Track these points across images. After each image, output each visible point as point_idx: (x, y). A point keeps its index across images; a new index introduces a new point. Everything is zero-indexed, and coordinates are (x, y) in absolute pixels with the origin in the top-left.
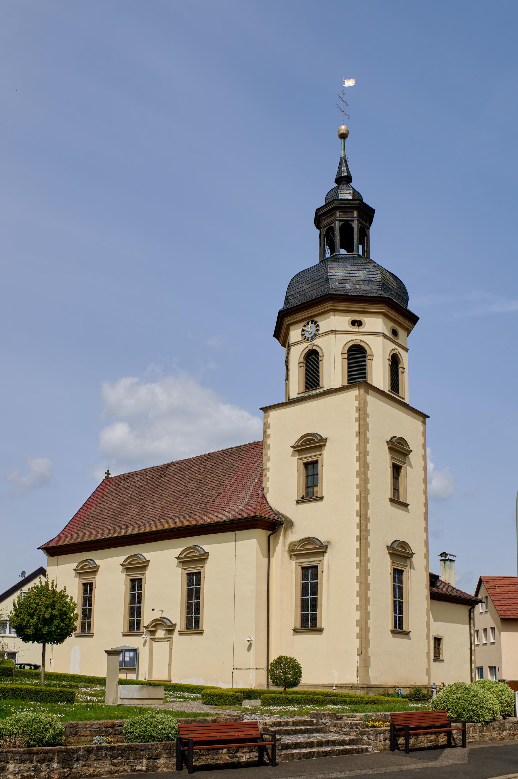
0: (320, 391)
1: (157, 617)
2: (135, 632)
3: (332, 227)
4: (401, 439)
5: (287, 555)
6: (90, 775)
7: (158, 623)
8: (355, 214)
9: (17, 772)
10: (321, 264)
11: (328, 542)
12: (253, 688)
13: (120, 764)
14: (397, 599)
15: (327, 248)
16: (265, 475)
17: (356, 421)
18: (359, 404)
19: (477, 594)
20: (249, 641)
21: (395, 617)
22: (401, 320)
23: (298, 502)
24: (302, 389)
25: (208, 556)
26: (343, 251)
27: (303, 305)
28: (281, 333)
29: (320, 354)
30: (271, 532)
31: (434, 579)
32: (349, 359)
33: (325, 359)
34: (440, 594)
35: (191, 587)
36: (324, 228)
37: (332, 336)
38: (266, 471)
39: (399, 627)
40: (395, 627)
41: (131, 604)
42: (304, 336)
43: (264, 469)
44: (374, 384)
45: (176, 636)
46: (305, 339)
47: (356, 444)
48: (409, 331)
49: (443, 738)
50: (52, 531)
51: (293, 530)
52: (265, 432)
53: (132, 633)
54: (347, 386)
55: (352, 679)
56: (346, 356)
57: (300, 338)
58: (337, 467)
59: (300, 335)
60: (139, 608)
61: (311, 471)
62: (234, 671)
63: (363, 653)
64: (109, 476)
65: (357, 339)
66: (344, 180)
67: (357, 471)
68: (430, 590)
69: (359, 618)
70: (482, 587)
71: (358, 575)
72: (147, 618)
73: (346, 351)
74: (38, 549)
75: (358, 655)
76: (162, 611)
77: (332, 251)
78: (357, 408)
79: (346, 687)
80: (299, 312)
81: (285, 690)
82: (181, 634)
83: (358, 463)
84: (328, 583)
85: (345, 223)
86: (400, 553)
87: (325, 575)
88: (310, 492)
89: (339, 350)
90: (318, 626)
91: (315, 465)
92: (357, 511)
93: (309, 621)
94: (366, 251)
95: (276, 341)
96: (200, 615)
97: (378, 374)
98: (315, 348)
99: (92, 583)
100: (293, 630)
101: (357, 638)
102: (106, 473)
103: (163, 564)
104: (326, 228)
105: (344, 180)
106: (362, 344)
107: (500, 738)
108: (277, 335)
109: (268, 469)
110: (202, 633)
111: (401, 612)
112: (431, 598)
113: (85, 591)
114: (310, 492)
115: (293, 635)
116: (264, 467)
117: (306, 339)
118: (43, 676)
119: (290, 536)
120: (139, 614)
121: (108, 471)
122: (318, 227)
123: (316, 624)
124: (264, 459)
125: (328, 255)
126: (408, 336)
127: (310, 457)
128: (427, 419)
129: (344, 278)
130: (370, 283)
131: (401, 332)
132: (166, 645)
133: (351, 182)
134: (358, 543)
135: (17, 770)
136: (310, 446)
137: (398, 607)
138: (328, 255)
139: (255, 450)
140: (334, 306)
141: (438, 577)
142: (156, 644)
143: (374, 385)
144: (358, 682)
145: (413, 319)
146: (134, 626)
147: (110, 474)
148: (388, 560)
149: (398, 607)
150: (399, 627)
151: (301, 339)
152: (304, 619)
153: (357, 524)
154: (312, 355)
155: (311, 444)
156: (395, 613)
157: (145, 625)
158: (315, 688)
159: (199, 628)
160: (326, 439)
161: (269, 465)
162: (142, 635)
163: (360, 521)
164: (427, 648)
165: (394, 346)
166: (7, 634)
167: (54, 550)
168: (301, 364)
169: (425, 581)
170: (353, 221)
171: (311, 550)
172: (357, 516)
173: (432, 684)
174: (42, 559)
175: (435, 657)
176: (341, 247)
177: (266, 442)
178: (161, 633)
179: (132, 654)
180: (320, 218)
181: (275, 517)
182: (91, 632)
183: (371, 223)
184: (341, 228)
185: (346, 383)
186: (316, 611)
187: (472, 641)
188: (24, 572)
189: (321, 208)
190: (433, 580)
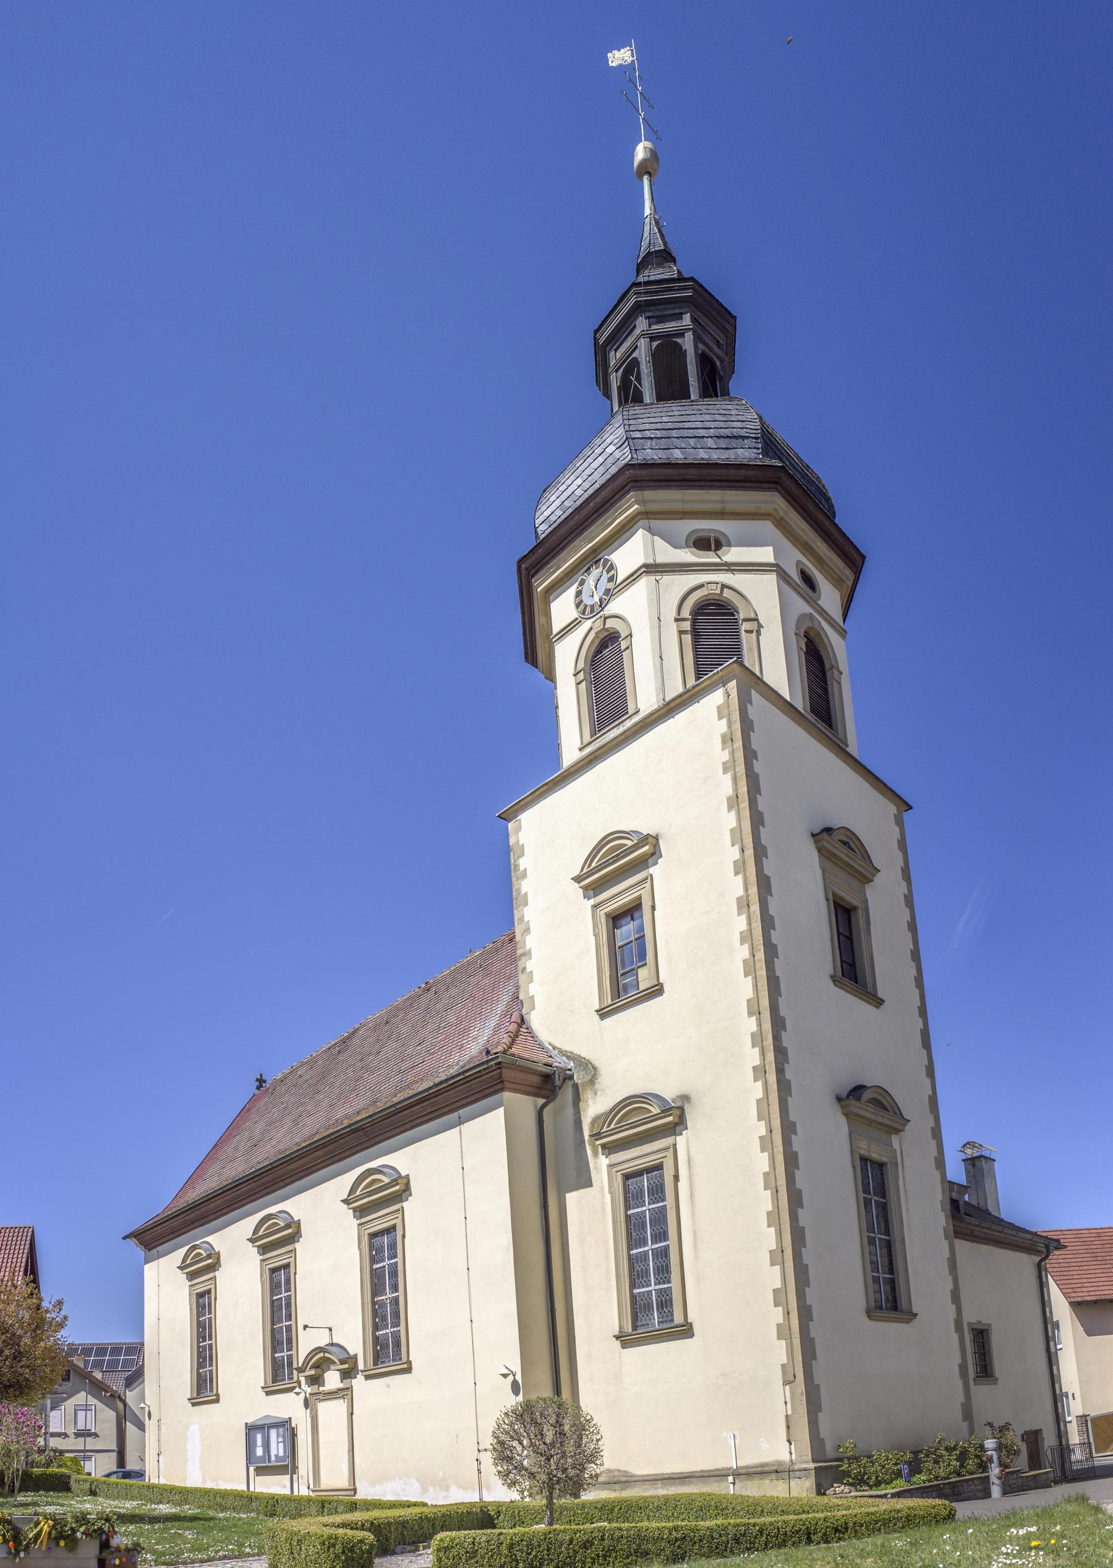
3: (635, 358)
7: (320, 1362)
8: (687, 320)
11: (685, 1098)
16: (524, 969)
18: (730, 724)
20: (505, 1376)
22: (822, 547)
23: (604, 1013)
24: (587, 738)
32: (696, 634)
35: (381, 1265)
36: (617, 371)
38: (523, 959)
39: (889, 1299)
42: (582, 607)
46: (583, 613)
51: (597, 1086)
56: (687, 625)
57: (574, 614)
59: (573, 606)
67: (739, 899)
74: (124, 1238)
75: (786, 1383)
76: (330, 1330)
81: (550, 1504)
84: (692, 1202)
88: (627, 971)
114: (627, 971)
116: (519, 952)
117: (588, 609)
119: (590, 1102)
124: (518, 930)
132: (338, 1407)
142: (324, 1408)
146: (279, 1374)
150: (889, 1299)
152: (638, 1309)
153: (753, 1035)
155: (618, 858)
158: (664, 1486)
170: (681, 335)
172: (750, 1014)
178: (332, 1380)
184: (656, 357)
186: (669, 1282)
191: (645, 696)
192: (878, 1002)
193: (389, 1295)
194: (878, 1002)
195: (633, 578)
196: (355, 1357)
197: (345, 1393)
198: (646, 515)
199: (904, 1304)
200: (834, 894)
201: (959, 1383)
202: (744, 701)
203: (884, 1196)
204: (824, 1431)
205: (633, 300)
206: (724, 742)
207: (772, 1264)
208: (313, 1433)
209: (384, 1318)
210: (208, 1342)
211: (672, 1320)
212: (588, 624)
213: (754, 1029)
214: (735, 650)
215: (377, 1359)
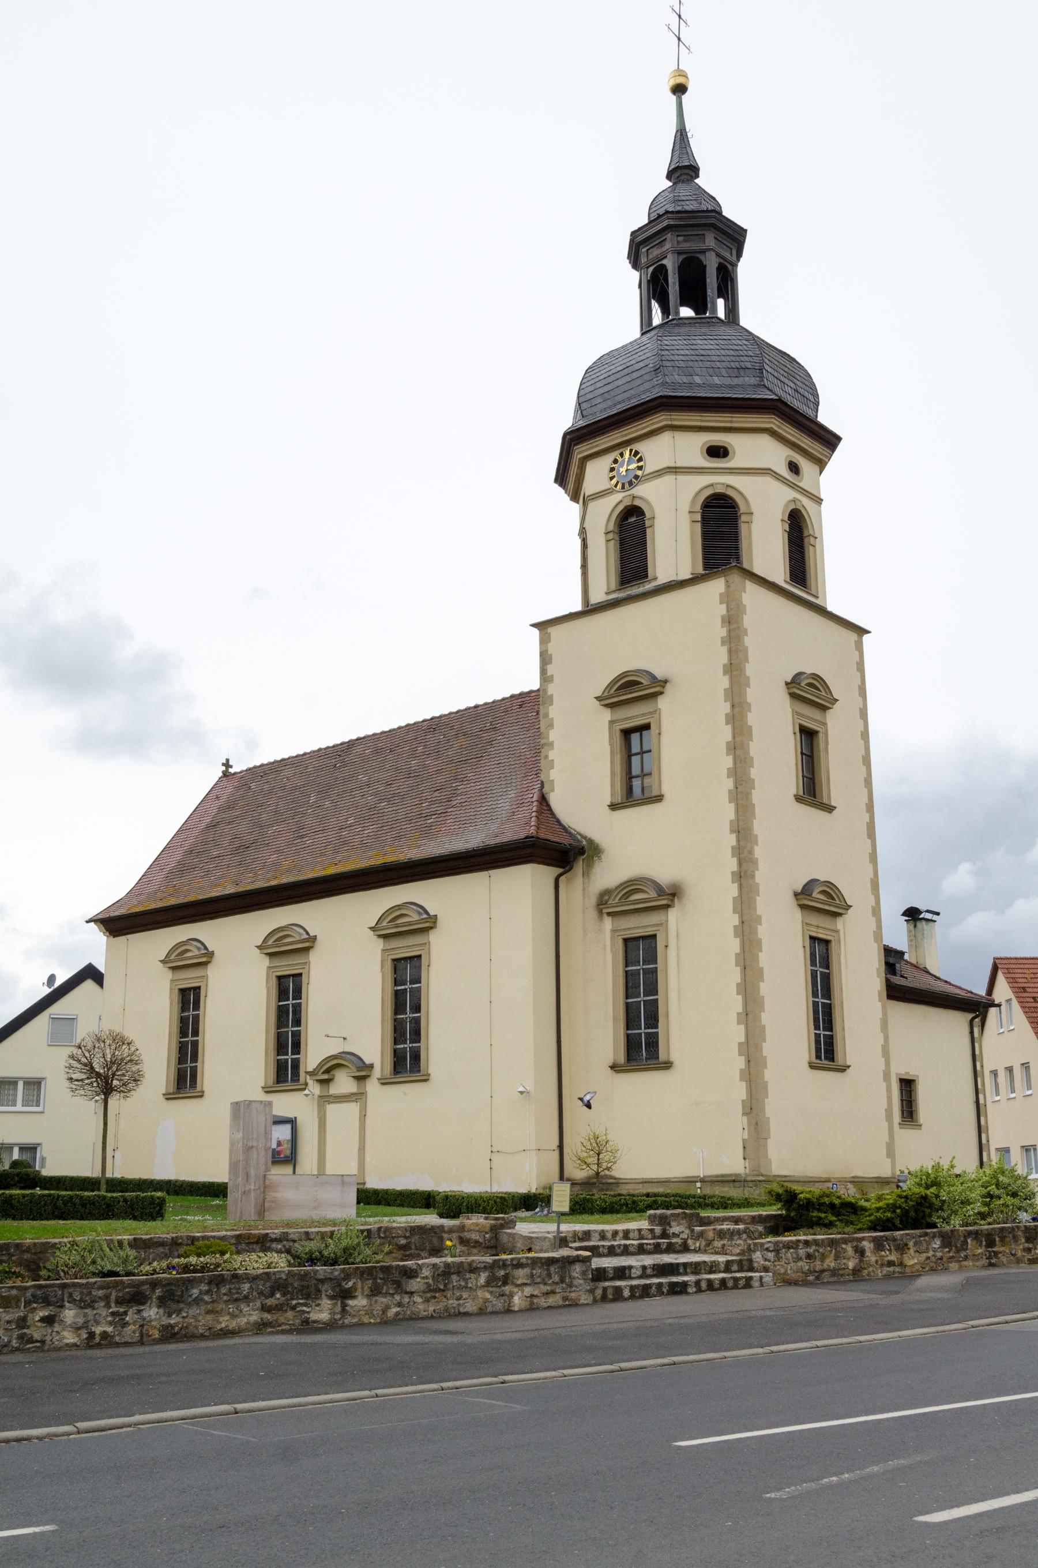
0: (648, 587)
1: (334, 1052)
4: (816, 677)
5: (592, 913)
6: (221, 1330)
9: (80, 1325)
10: (645, 337)
12: (533, 1191)
13: (279, 1308)
15: (655, 307)
16: (546, 757)
17: (723, 643)
19: (990, 990)
21: (817, 1036)
22: (806, 442)
23: (614, 807)
24: (613, 586)
25: (435, 923)
26: (686, 312)
27: (604, 424)
28: (568, 474)
29: (648, 515)
30: (561, 870)
31: (892, 959)
32: (705, 521)
33: (658, 523)
34: (906, 986)
37: (669, 479)
39: (826, 1052)
40: (818, 1057)
41: (278, 1027)
43: (543, 746)
44: (757, 570)
45: (372, 1087)
46: (616, 486)
48: (821, 464)
49: (913, 1258)
50: (116, 884)
52: (543, 672)
53: (282, 1086)
54: (702, 575)
55: (733, 1163)
56: (698, 517)
58: (687, 738)
60: (297, 1036)
61: (633, 742)
62: (494, 1157)
63: (753, 1108)
64: (231, 770)
65: (720, 482)
66: (684, 171)
68: (887, 980)
69: (743, 1039)
70: (1001, 978)
71: (738, 951)
72: (313, 1056)
73: (698, 508)
74: (87, 922)
75: (744, 1114)
77: (665, 310)
78: (723, 618)
80: (604, 433)
82: (384, 1082)
83: (730, 726)
85: (688, 253)
86: (820, 901)
87: (672, 952)
88: (634, 788)
89: (685, 505)
90: (662, 1057)
91: (644, 733)
92: (731, 821)
93: (642, 1046)
94: (732, 310)
95: (561, 491)
96: (422, 1044)
97: (765, 548)
98: (637, 503)
99: (199, 988)
100: (612, 1067)
101: (741, 1080)
102: (223, 764)
103: (345, 938)
104: (651, 269)
105: (684, 171)
106: (730, 492)
107: (1029, 1260)
108: (561, 478)
109: (551, 745)
111: (829, 1025)
112: (890, 997)
113: (184, 1005)
114: (634, 788)
115: (812, 1066)
117: (627, 485)
118: (103, 1182)
120: (297, 1047)
121: (228, 760)
122: (635, 264)
123: (658, 1054)
125: (657, 318)
126: (821, 473)
127: (634, 715)
128: (866, 637)
129: (691, 364)
130: (742, 372)
131: (804, 464)
133: (697, 176)
134: (736, 885)
135: (80, 1321)
136: (633, 693)
137: (824, 1017)
138: (657, 318)
139: (526, 708)
140: (671, 420)
141: (902, 953)
142: (333, 1110)
143: (829, 609)
144: (747, 1171)
145: (830, 440)
146: (286, 1072)
147: (231, 767)
148: (797, 915)
149: (824, 1017)
150: (826, 1052)
151: (608, 487)
152: (632, 1046)
153: (733, 848)
154: (632, 515)
156: (817, 1027)
157: (310, 1069)
159: (419, 1071)
160: (666, 682)
161: (553, 735)
162: (304, 1089)
163: (738, 841)
164: (885, 1099)
165: (792, 494)
166: (19, 1107)
167: (117, 924)
168: (611, 536)
169: (875, 962)
170: (704, 252)
171: (642, 908)
172: (732, 831)
173: (898, 1173)
174: (96, 947)
176: (683, 303)
177: (545, 691)
178: (344, 1083)
180: (640, 246)
181: (565, 840)
182: (199, 1089)
183: (739, 254)
185: (700, 570)
186: (657, 1027)
187: (980, 1086)
188: (52, 979)
189: (640, 229)
190: (892, 960)
192: (829, 809)
193: (409, 1015)
194: (829, 809)
195: (659, 473)
196: (371, 1066)
197: (359, 1097)
200: (800, 725)
201: (885, 1125)
203: (828, 967)
205: (665, 223)
206: (723, 622)
207: (738, 1023)
208: (319, 1131)
209: (404, 1033)
210: (190, 1038)
211: (658, 1058)
212: (618, 497)
213: (734, 843)
214: (738, 558)
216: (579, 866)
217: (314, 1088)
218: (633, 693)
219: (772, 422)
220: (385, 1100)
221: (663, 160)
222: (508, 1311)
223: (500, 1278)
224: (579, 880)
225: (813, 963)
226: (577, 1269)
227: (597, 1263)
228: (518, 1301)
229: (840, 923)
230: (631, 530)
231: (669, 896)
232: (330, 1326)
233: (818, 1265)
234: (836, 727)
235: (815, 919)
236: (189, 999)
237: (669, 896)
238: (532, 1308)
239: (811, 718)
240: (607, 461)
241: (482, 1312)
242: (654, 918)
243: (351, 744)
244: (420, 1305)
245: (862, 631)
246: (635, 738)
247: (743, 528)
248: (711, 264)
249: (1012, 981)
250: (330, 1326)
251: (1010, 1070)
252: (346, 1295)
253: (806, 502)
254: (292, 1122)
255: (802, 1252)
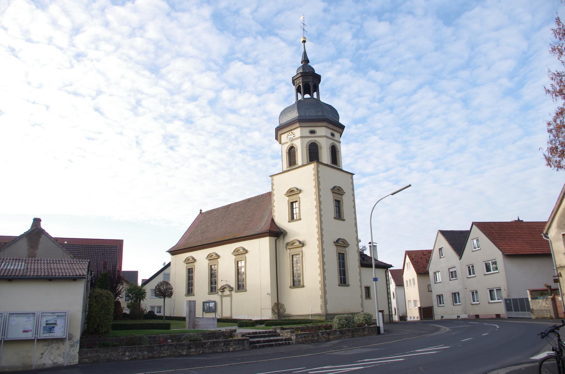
0: (296, 166)
2: (214, 293)
7: (223, 289)
14: (342, 269)
22: (336, 128)
39: (343, 281)
47: (114, 248)
50: (173, 243)
52: (272, 188)
66: (306, 61)
79: (316, 315)
85: (308, 81)
86: (341, 244)
97: (325, 156)
105: (306, 61)
108: (277, 138)
109: (274, 206)
110: (246, 291)
115: (339, 285)
127: (293, 198)
131: (336, 133)
132: (229, 298)
139: (268, 196)
145: (342, 127)
146: (213, 289)
150: (343, 281)
165: (332, 141)
167: (174, 252)
174: (168, 258)
175: (366, 297)
178: (227, 292)
179: (214, 303)
181: (278, 230)
188: (164, 263)
191: (299, 162)
192: (344, 220)
194: (344, 220)
195: (298, 138)
197: (230, 296)
198: (300, 127)
199: (347, 283)
202: (318, 167)
204: (328, 308)
215: (238, 289)
216: (282, 237)
217: (220, 293)
218: (293, 193)
219: (325, 124)
220: (236, 295)
221: (300, 59)
222: (229, 351)
223: (227, 344)
224: (282, 241)
225: (339, 259)
226: (246, 342)
227: (251, 340)
228: (231, 349)
229: (347, 249)
230: (291, 152)
231: (302, 244)
232: (186, 355)
233: (307, 339)
234: (345, 200)
235: (340, 248)
236: (190, 272)
237: (302, 244)
238: (234, 351)
239: (338, 197)
240: (286, 135)
241: (222, 352)
242: (299, 249)
243: (230, 205)
244: (207, 351)
245: (353, 174)
246: (294, 204)
247: (319, 151)
248: (311, 84)
249: (410, 257)
250: (186, 355)
251: (410, 280)
252: (190, 348)
253: (336, 143)
254: (215, 302)
255: (303, 336)
